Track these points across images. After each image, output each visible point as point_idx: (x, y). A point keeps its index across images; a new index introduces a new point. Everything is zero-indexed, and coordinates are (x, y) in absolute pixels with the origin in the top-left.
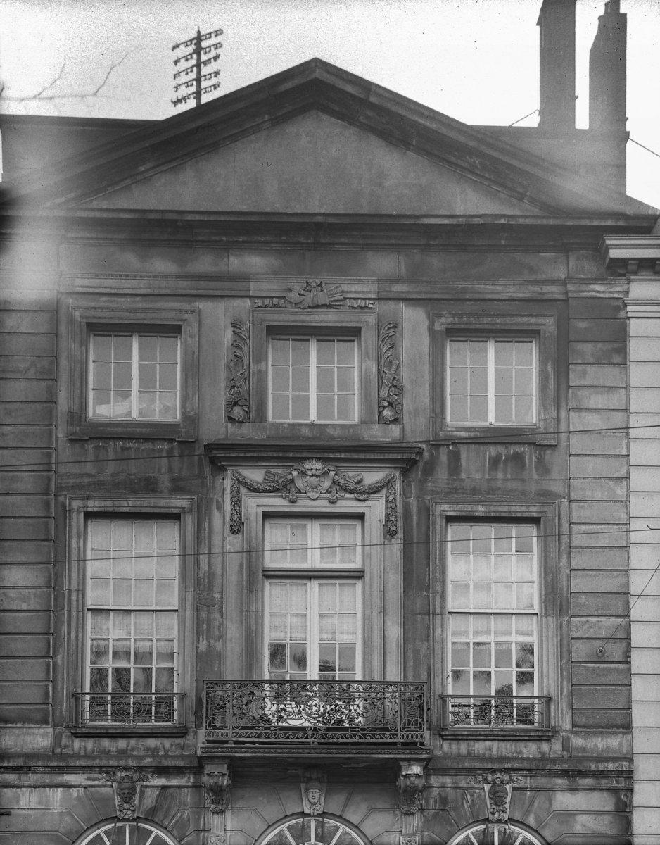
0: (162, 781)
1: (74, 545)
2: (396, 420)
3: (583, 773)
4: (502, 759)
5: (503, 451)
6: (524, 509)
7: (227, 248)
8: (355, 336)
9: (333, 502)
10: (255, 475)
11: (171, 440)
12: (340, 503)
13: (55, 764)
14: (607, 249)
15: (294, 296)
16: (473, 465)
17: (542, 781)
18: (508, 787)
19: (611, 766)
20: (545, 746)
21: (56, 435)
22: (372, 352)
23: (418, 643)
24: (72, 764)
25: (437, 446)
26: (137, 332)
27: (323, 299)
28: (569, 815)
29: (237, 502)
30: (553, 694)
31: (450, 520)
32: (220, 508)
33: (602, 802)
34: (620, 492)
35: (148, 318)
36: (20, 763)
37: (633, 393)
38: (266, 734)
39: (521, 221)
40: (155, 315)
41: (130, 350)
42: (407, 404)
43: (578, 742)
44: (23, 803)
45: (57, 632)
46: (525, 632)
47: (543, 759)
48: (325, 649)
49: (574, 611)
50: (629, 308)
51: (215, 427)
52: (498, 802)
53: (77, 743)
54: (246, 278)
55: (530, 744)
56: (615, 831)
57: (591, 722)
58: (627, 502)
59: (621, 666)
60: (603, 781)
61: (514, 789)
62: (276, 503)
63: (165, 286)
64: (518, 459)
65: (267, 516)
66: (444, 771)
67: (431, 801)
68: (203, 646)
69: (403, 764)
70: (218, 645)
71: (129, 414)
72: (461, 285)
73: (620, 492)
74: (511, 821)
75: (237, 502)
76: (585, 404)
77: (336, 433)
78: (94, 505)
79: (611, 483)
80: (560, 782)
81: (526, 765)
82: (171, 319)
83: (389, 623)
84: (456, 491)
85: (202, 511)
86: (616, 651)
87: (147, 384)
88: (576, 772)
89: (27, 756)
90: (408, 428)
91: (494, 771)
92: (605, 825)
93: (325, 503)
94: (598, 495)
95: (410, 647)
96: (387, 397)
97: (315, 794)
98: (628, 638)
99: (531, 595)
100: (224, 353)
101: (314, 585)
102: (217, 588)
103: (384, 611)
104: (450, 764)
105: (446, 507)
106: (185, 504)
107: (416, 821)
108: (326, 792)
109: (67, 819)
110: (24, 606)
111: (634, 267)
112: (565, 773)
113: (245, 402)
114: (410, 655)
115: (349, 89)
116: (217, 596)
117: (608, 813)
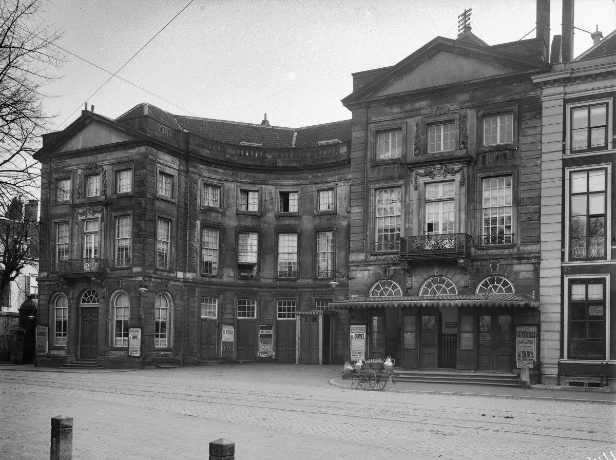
0: (395, 268)
1: (372, 199)
2: (465, 148)
3: (523, 258)
4: (497, 255)
5: (500, 153)
6: (506, 172)
7: (414, 101)
10: (422, 171)
11: (398, 163)
12: (447, 177)
13: (366, 263)
14: (532, 80)
15: (434, 113)
16: (490, 159)
17: (510, 262)
18: (498, 264)
19: (532, 255)
20: (511, 250)
22: (458, 127)
23: (471, 220)
24: (370, 264)
25: (478, 154)
27: (442, 112)
28: (518, 273)
29: (416, 180)
30: (515, 233)
31: (482, 178)
32: (412, 183)
33: (530, 267)
34: (538, 162)
35: (394, 126)
36: (356, 264)
37: (543, 128)
39: (503, 76)
40: (394, 126)
41: (441, 129)
42: (469, 142)
43: (522, 248)
44: (358, 275)
45: (367, 226)
46: (509, 213)
47: (511, 254)
48: (444, 224)
49: (522, 204)
50: (542, 98)
51: (411, 157)
52: (495, 269)
53: (372, 257)
54: (420, 109)
55: (506, 250)
56: (533, 277)
57: (526, 241)
58: (540, 165)
59: (538, 221)
60: (530, 261)
61: (500, 265)
62: (427, 179)
63: (396, 116)
64: (505, 155)
65: (426, 184)
66: (477, 260)
67: (474, 270)
68: (407, 226)
69: (458, 259)
70: (411, 225)
71: (388, 157)
72: (486, 100)
73: (538, 162)
74: (499, 275)
75: (416, 180)
76: (527, 134)
77: (446, 154)
78: (377, 186)
79: (535, 160)
80: (516, 262)
81: (503, 257)
82: (398, 126)
83: (461, 214)
84: (484, 168)
85: (407, 184)
86: (536, 217)
87: (393, 147)
88: (520, 258)
89: (359, 262)
90: (469, 150)
91: (493, 259)
92: (530, 275)
94: (531, 164)
95: (469, 221)
96: (463, 142)
97: (437, 270)
98: (540, 212)
99: (510, 199)
100: (414, 135)
101: (441, 204)
102: (411, 208)
103: (460, 210)
104: (479, 258)
105: (480, 174)
106: (402, 183)
107: (468, 277)
108: (442, 269)
109: (369, 280)
110: (358, 218)
111: (543, 84)
112: (517, 259)
113: (421, 148)
114: (469, 223)
115: (449, 43)
116: (411, 210)
117: (530, 271)
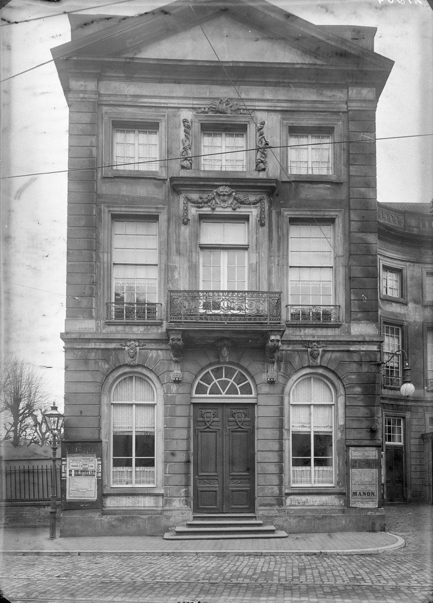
8: (329, 133)
9: (234, 209)
21: (220, 186)
26: (311, 133)
38: (201, 318)
93: (230, 209)
